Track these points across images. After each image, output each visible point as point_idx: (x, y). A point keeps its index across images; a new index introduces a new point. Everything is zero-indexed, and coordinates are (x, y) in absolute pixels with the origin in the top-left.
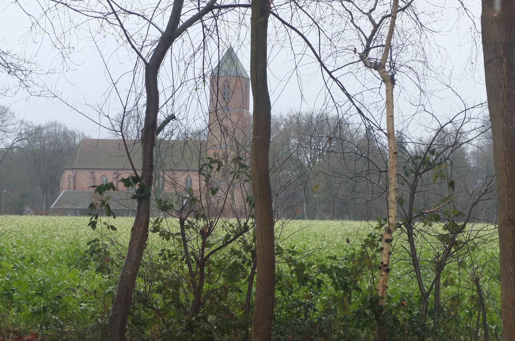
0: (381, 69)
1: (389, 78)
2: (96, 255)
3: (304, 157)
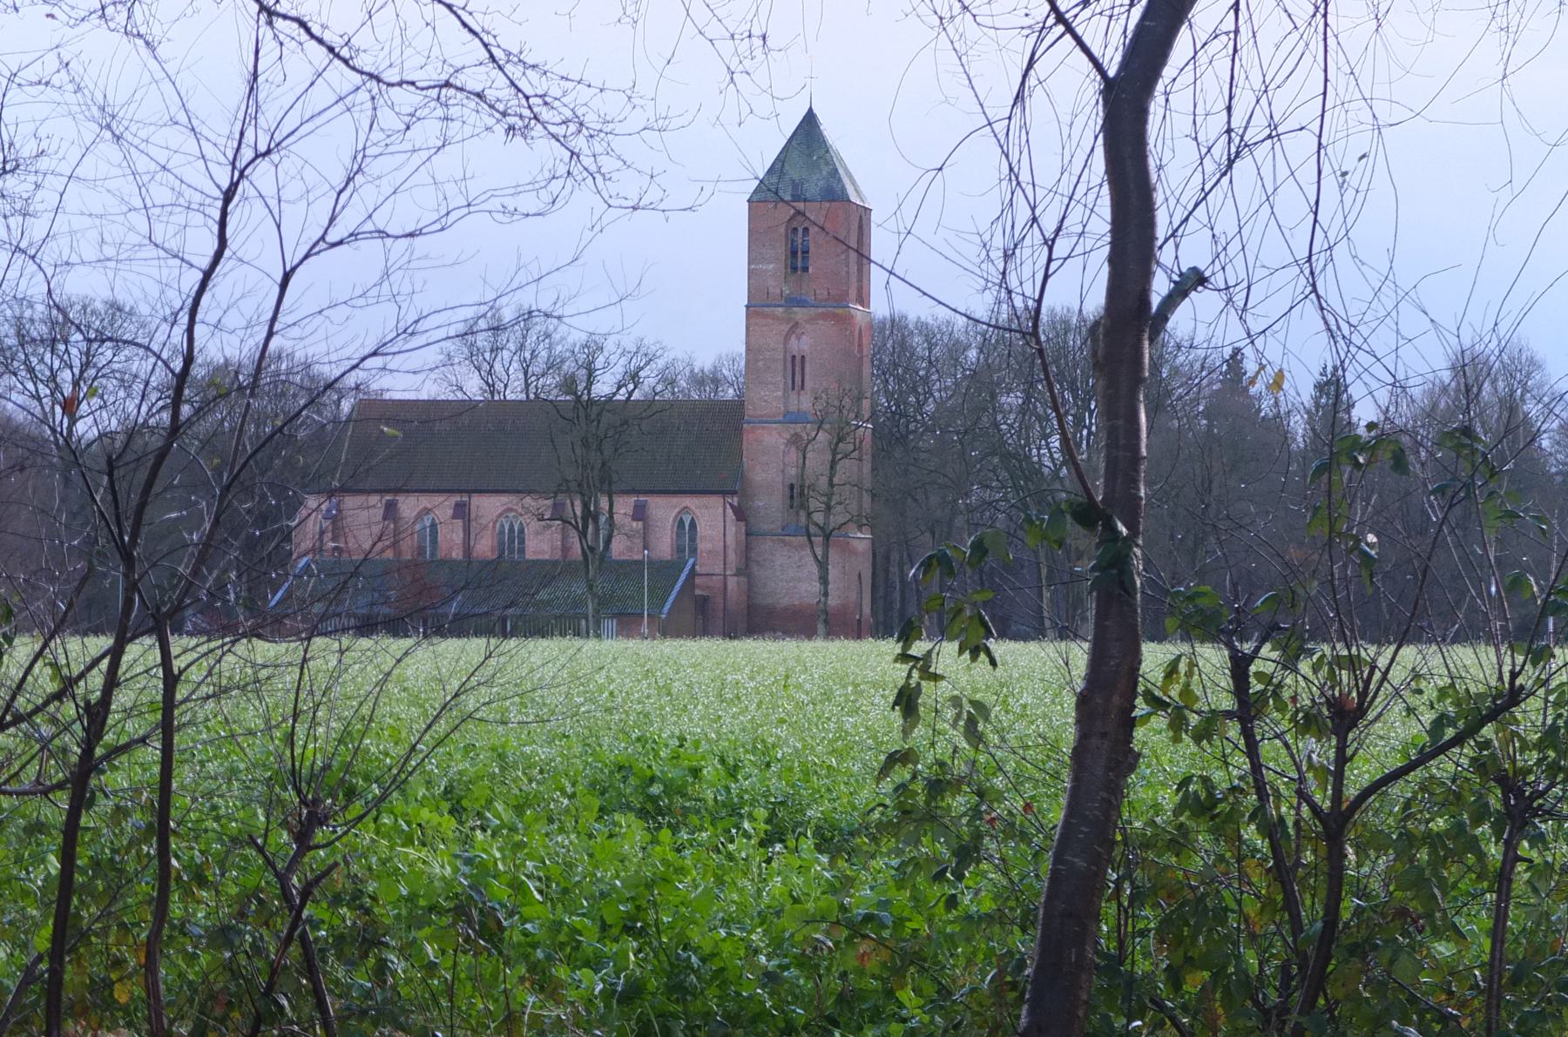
2: (927, 807)
3: (1039, 449)
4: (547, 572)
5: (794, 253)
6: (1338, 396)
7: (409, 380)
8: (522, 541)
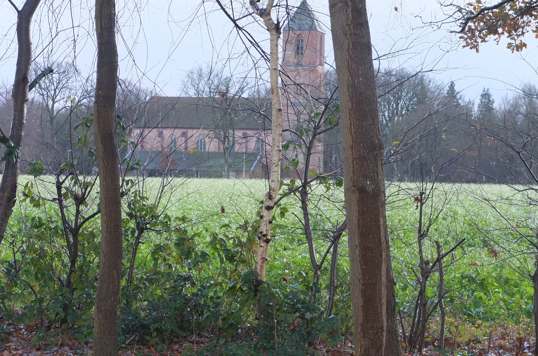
0: (266, 16)
1: (274, 26)
4: (210, 156)
5: (298, 48)
6: (489, 99)
7: (171, 90)
8: (205, 145)
